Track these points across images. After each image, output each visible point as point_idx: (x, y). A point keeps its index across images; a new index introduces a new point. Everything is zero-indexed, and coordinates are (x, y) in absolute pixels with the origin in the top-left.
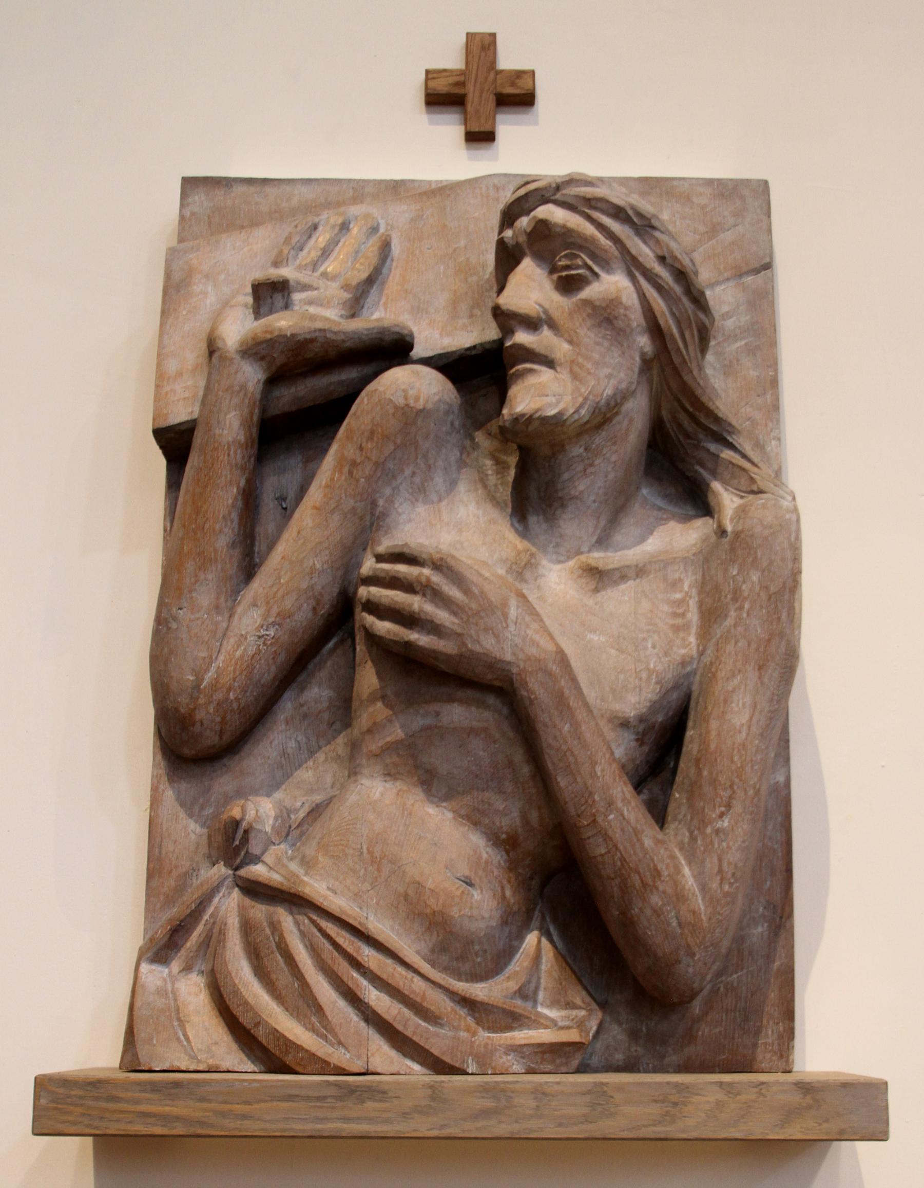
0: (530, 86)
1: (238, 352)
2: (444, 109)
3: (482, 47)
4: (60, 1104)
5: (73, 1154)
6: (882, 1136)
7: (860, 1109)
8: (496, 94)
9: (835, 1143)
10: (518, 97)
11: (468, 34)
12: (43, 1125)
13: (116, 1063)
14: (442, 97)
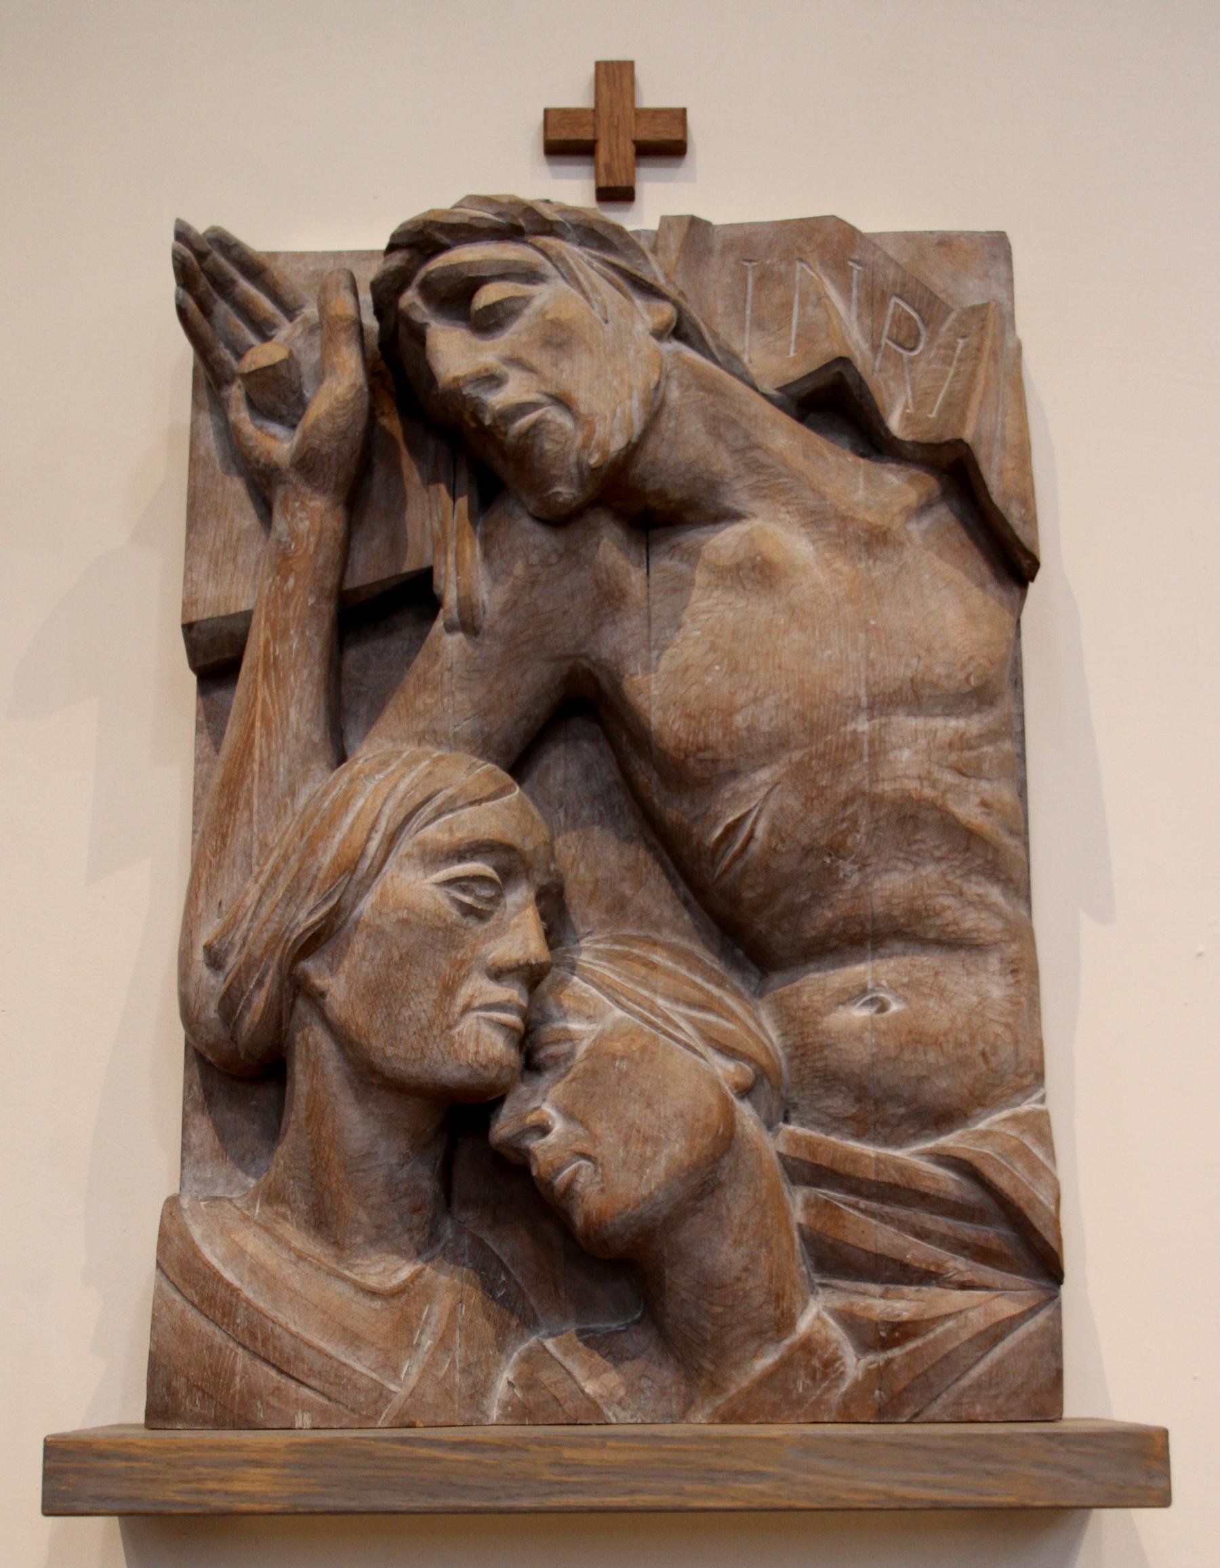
0: (679, 137)
1: (292, 465)
2: (578, 159)
3: (614, 77)
4: (73, 1475)
5: (97, 1545)
6: (1163, 1499)
7: (1137, 1466)
8: (635, 142)
9: (1095, 1512)
10: (666, 145)
11: (598, 64)
12: (56, 1503)
13: (138, 1416)
14: (565, 143)
